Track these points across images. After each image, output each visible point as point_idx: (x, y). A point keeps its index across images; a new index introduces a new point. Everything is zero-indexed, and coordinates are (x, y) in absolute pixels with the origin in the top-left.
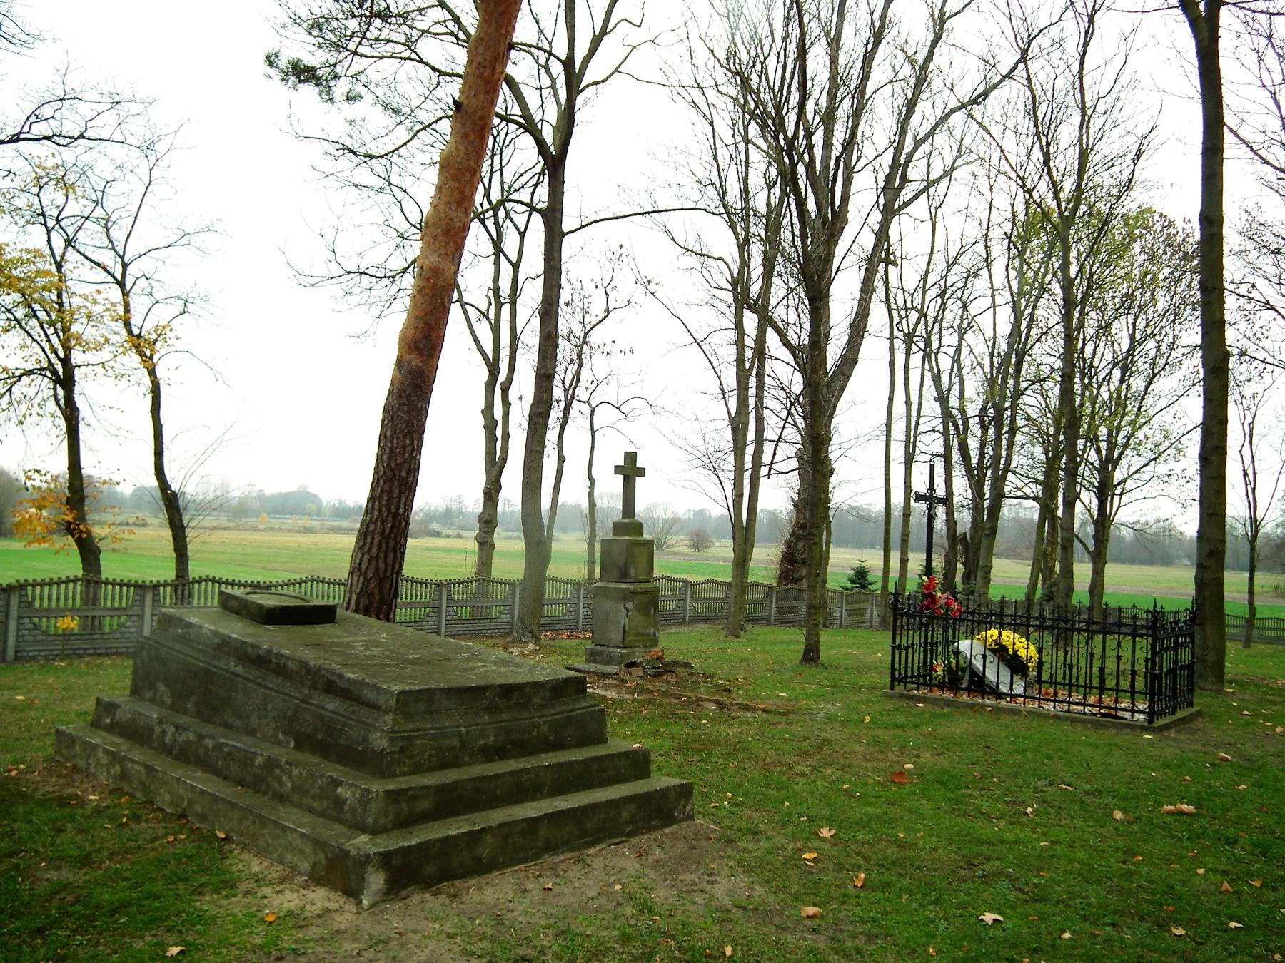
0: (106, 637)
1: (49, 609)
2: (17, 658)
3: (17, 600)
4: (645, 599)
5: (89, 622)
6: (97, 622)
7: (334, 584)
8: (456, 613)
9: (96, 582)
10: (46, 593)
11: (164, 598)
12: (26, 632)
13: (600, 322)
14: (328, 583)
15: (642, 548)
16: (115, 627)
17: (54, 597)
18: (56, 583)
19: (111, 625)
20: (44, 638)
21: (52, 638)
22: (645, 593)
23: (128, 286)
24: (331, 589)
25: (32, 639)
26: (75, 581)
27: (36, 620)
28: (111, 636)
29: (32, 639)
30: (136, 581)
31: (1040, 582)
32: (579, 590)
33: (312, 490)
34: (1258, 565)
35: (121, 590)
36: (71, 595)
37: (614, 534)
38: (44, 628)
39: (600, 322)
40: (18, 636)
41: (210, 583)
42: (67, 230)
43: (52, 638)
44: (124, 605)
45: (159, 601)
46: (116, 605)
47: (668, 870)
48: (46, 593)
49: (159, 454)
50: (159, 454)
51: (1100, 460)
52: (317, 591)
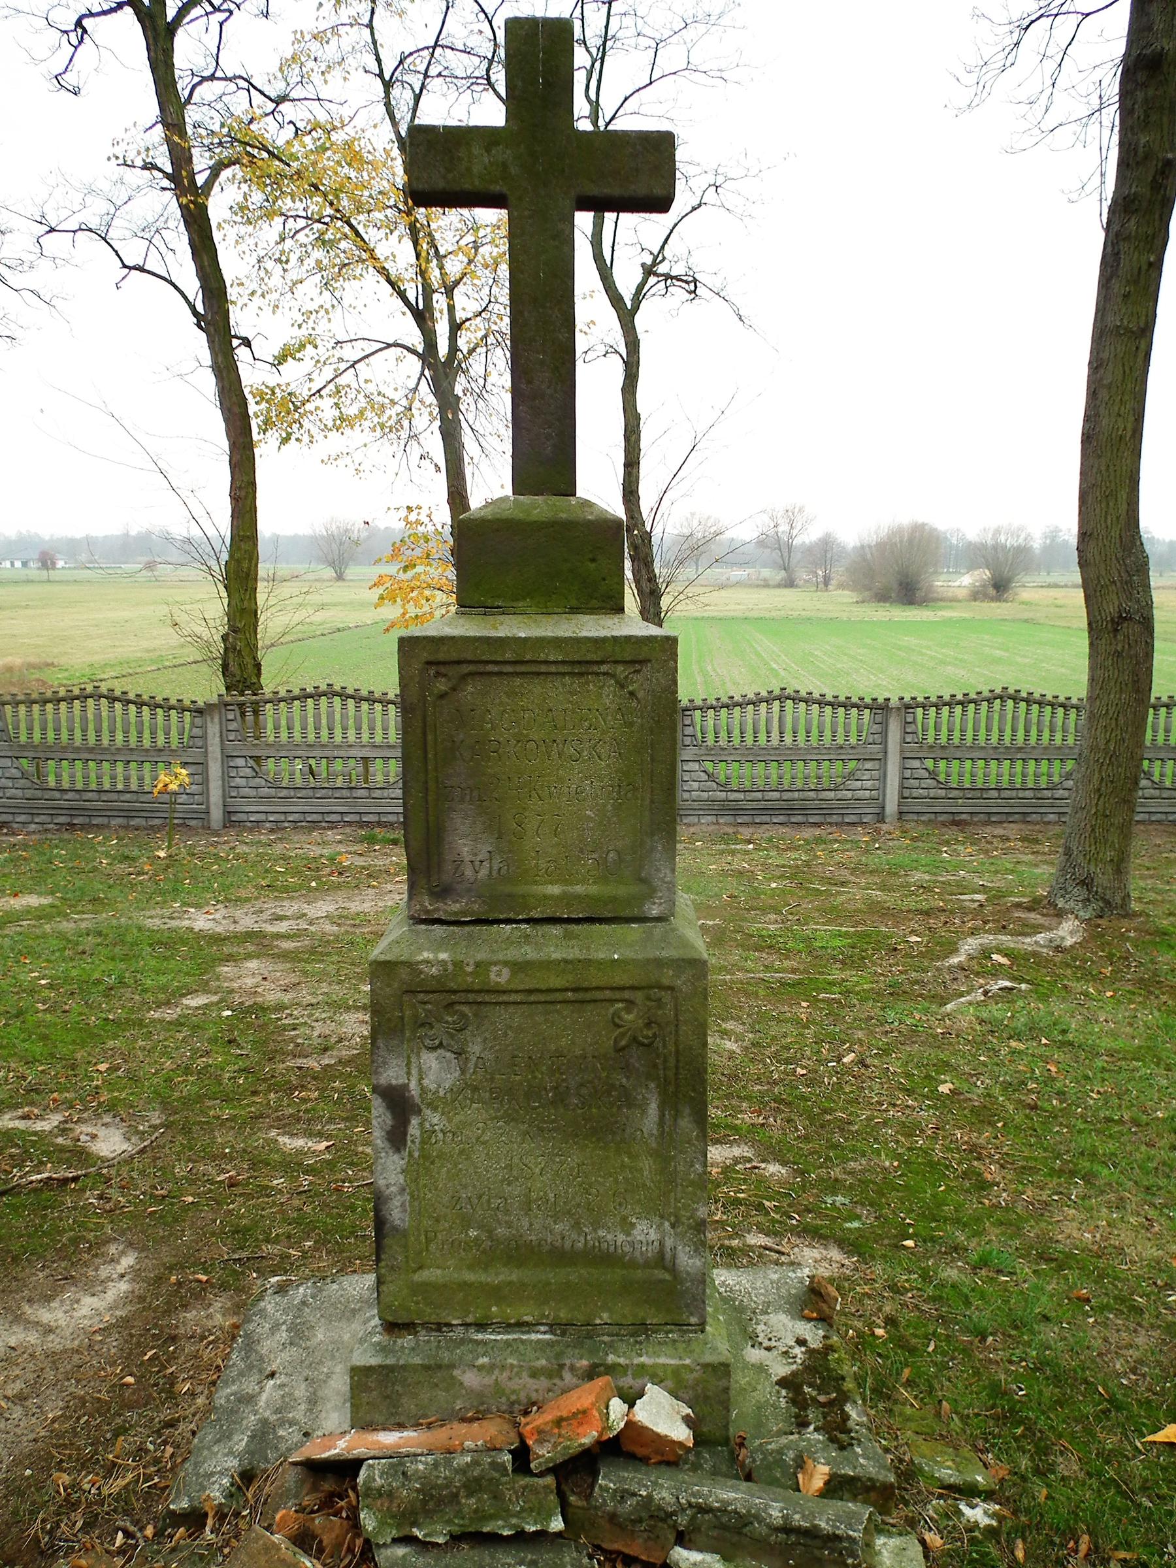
0: (377, 793)
1: (795, 748)
2: (231, 821)
3: (217, 729)
7: (1052, 705)
8: (933, 775)
12: (242, 782)
13: (418, 51)
14: (1028, 701)
16: (1056, 779)
18: (961, 703)
21: (284, 793)
24: (828, 719)
25: (253, 793)
26: (386, 703)
28: (386, 793)
29: (253, 793)
32: (885, 725)
33: (920, 521)
35: (29, 712)
36: (324, 721)
39: (418, 51)
40: (902, 787)
41: (1010, 703)
43: (284, 793)
47: (568, 1447)
51: (167, 176)
52: (795, 721)
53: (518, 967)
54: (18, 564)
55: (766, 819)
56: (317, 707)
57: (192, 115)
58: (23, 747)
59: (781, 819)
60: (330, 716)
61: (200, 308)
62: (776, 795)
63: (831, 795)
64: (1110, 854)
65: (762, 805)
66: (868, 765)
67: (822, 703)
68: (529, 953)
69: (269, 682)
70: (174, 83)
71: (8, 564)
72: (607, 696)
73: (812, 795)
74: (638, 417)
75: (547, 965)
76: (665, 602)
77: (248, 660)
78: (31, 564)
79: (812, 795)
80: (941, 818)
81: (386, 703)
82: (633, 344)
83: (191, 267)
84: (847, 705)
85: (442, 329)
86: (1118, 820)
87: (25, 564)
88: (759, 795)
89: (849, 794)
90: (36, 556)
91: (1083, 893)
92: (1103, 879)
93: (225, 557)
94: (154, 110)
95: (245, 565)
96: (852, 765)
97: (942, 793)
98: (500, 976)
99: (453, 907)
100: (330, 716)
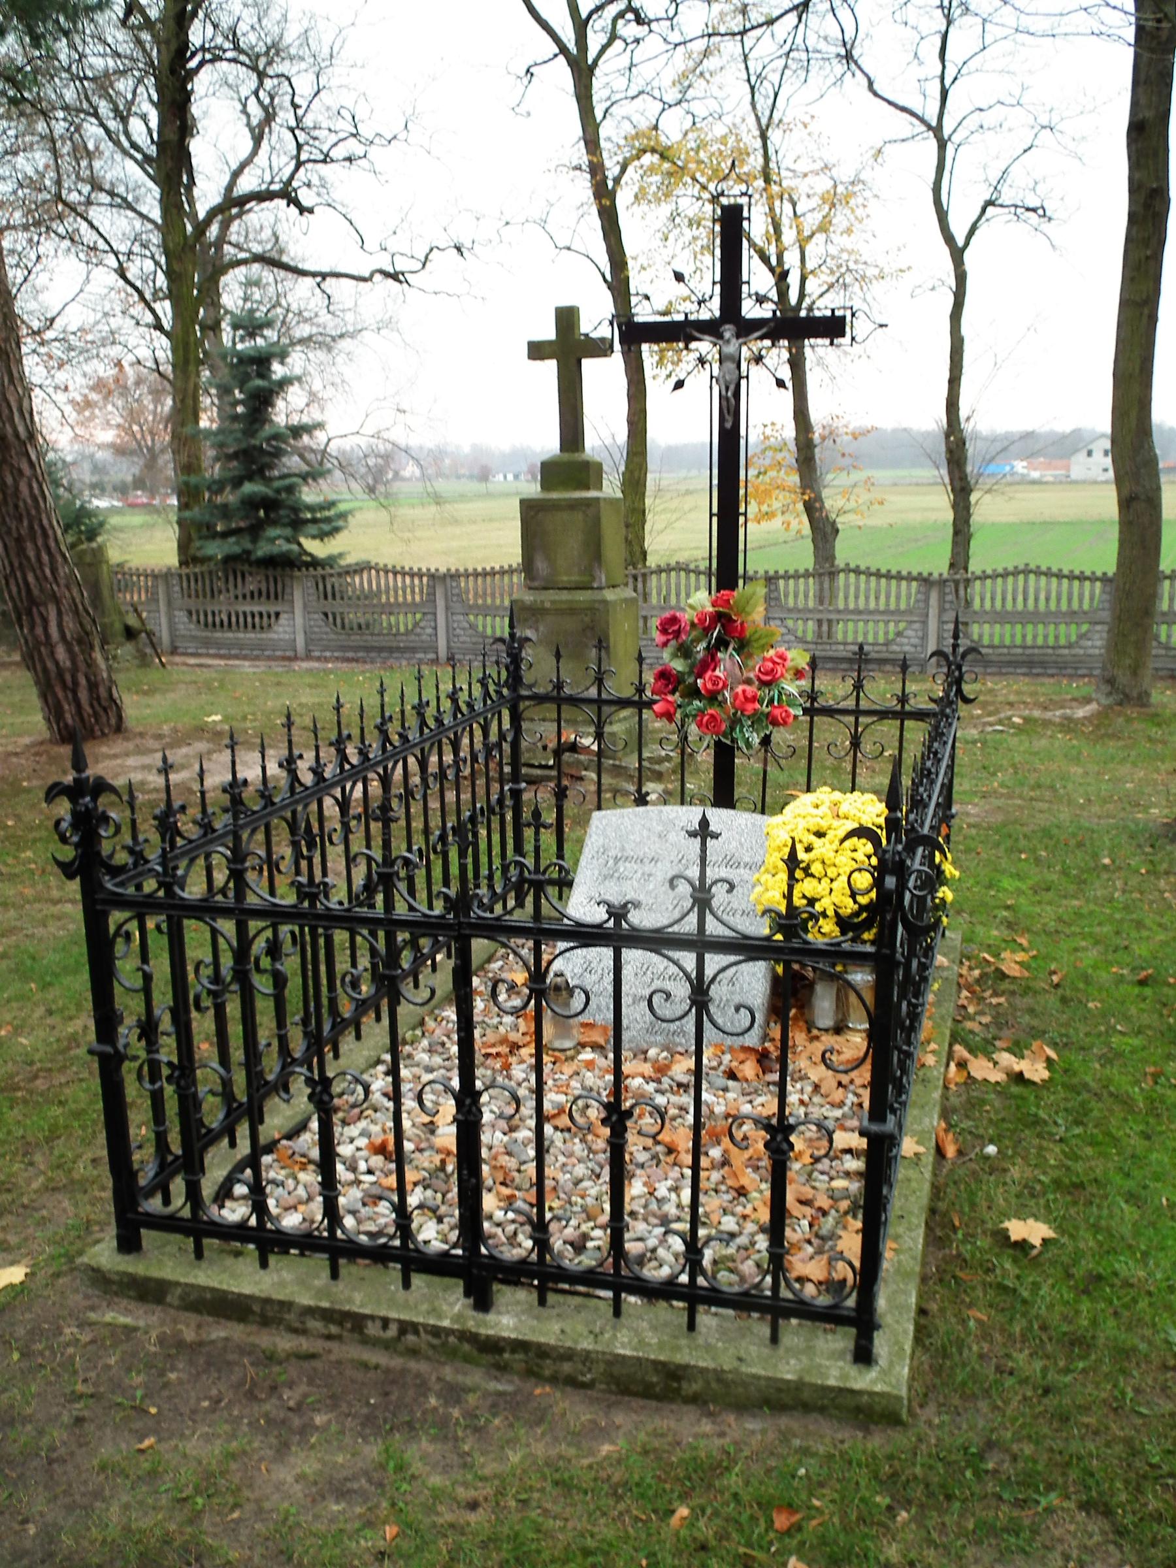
1: (1036, 613)
4: (570, 624)
5: (825, 628)
6: (825, 628)
9: (644, 575)
10: (802, 588)
11: (786, 595)
15: (565, 516)
17: (1054, 595)
19: (886, 633)
20: (1163, 652)
22: (572, 610)
23: (946, 132)
26: (698, 573)
27: (790, 623)
30: (920, 574)
31: (933, 612)
34: (790, 456)
37: (546, 485)
38: (480, 628)
42: (151, 216)
44: (1086, 606)
45: (778, 599)
46: (872, 605)
48: (802, 588)
49: (954, 381)
50: (954, 381)
53: (553, 602)
54: (510, 477)
55: (1011, 670)
56: (669, 578)
57: (603, 132)
58: (471, 607)
59: (1023, 670)
60: (678, 585)
61: (609, 277)
62: (1019, 651)
63: (1066, 651)
64: (1128, 661)
65: (1008, 658)
66: (1098, 628)
67: (1060, 576)
68: (557, 598)
69: (652, 561)
70: (592, 109)
71: (501, 477)
72: (579, 516)
73: (1050, 651)
74: (961, 340)
75: (561, 602)
76: (973, 498)
77: (637, 549)
78: (522, 477)
79: (1050, 651)
80: (1161, 673)
81: (698, 573)
82: (961, 278)
83: (603, 246)
84: (1082, 578)
85: (793, 280)
86: (1133, 638)
87: (516, 477)
88: (1005, 651)
89: (1081, 652)
90: (525, 469)
91: (1108, 688)
92: (1123, 678)
93: (622, 468)
94: (579, 132)
95: (636, 474)
96: (1085, 627)
97: (1163, 652)
98: (547, 605)
99: (536, 584)
100: (678, 585)
